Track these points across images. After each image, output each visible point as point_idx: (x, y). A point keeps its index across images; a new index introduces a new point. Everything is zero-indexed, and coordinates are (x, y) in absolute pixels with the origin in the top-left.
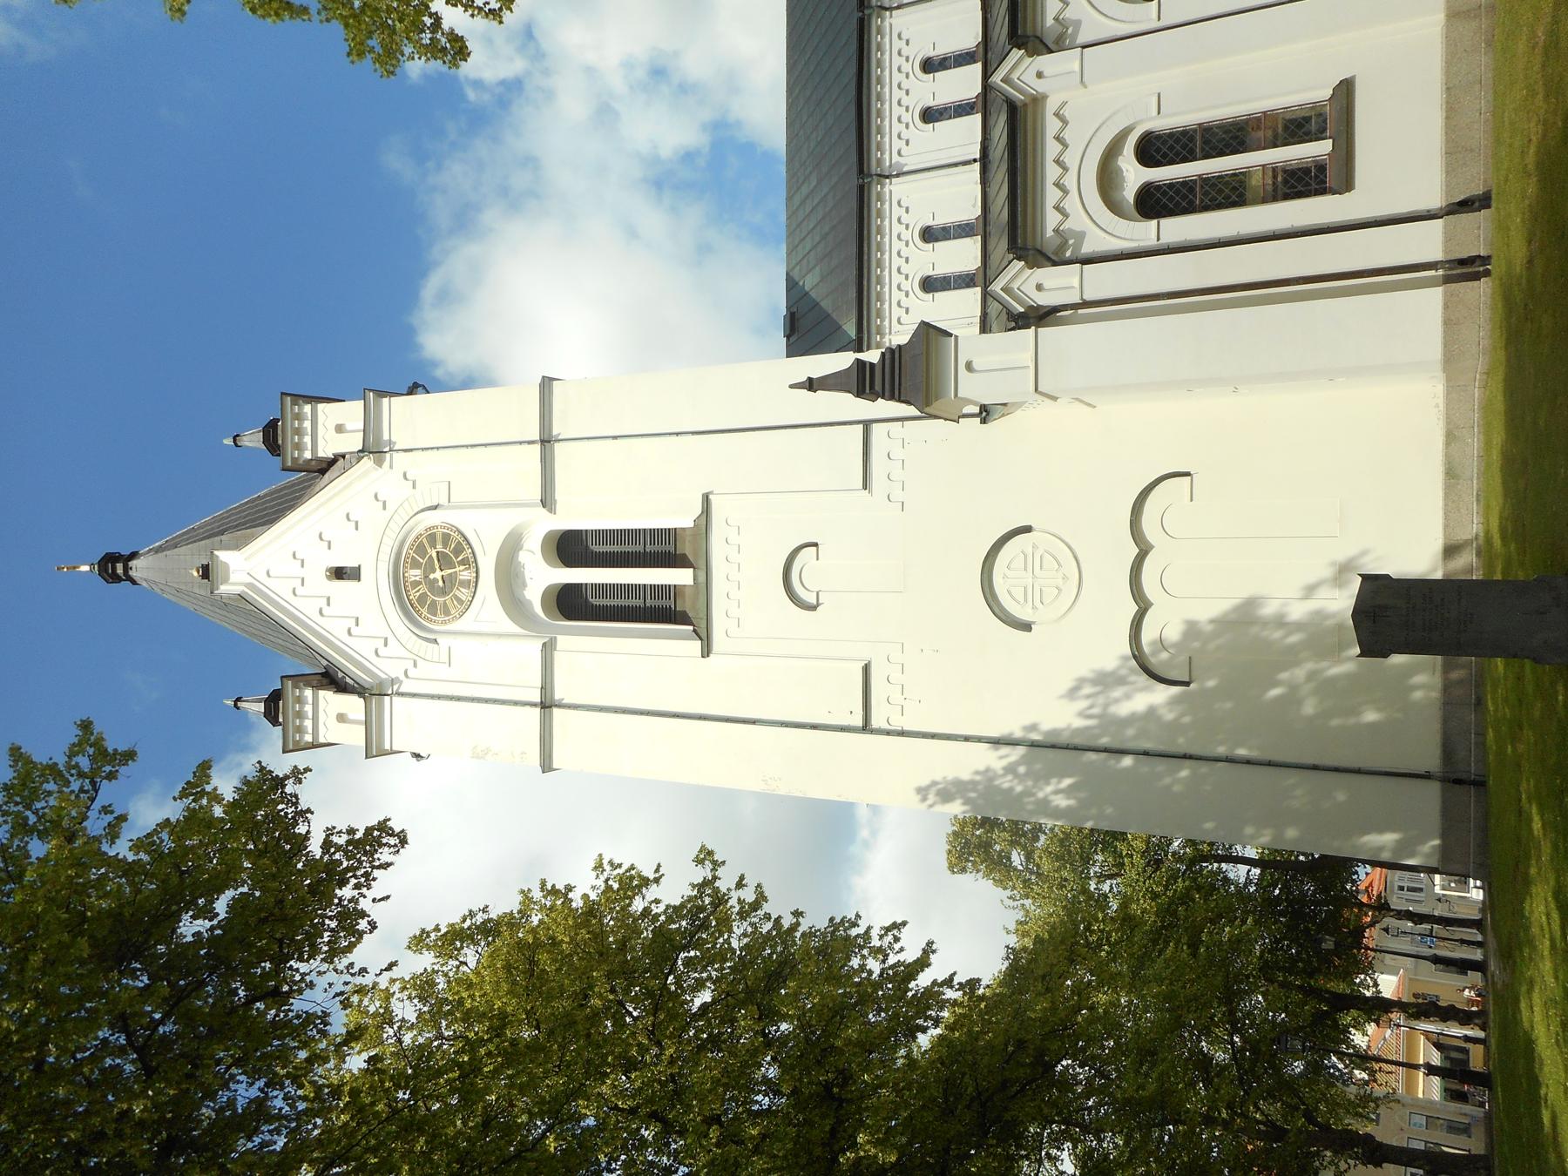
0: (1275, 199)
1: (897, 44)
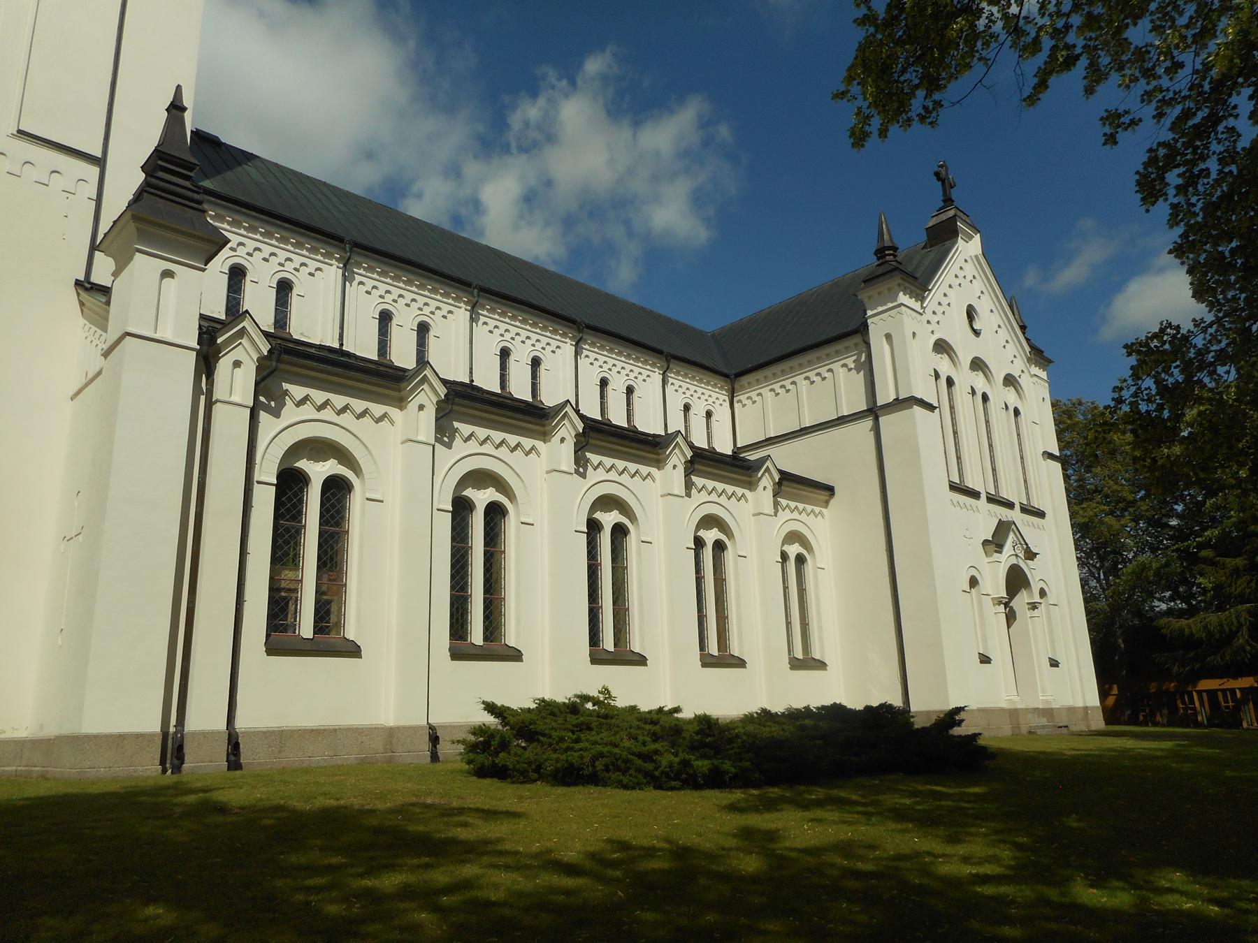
0: (271, 589)
1: (446, 308)
